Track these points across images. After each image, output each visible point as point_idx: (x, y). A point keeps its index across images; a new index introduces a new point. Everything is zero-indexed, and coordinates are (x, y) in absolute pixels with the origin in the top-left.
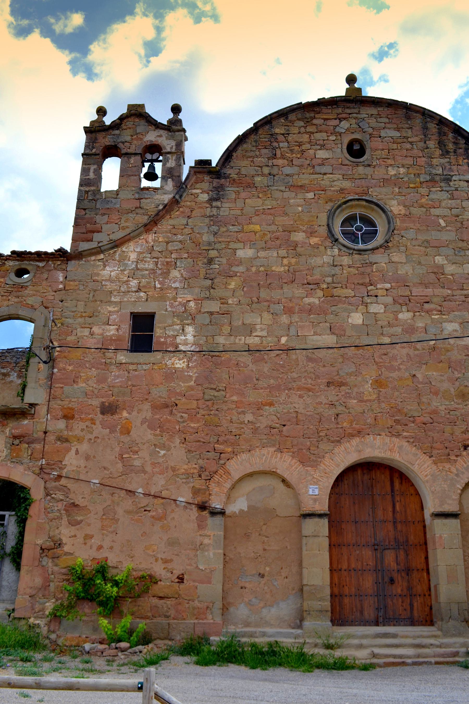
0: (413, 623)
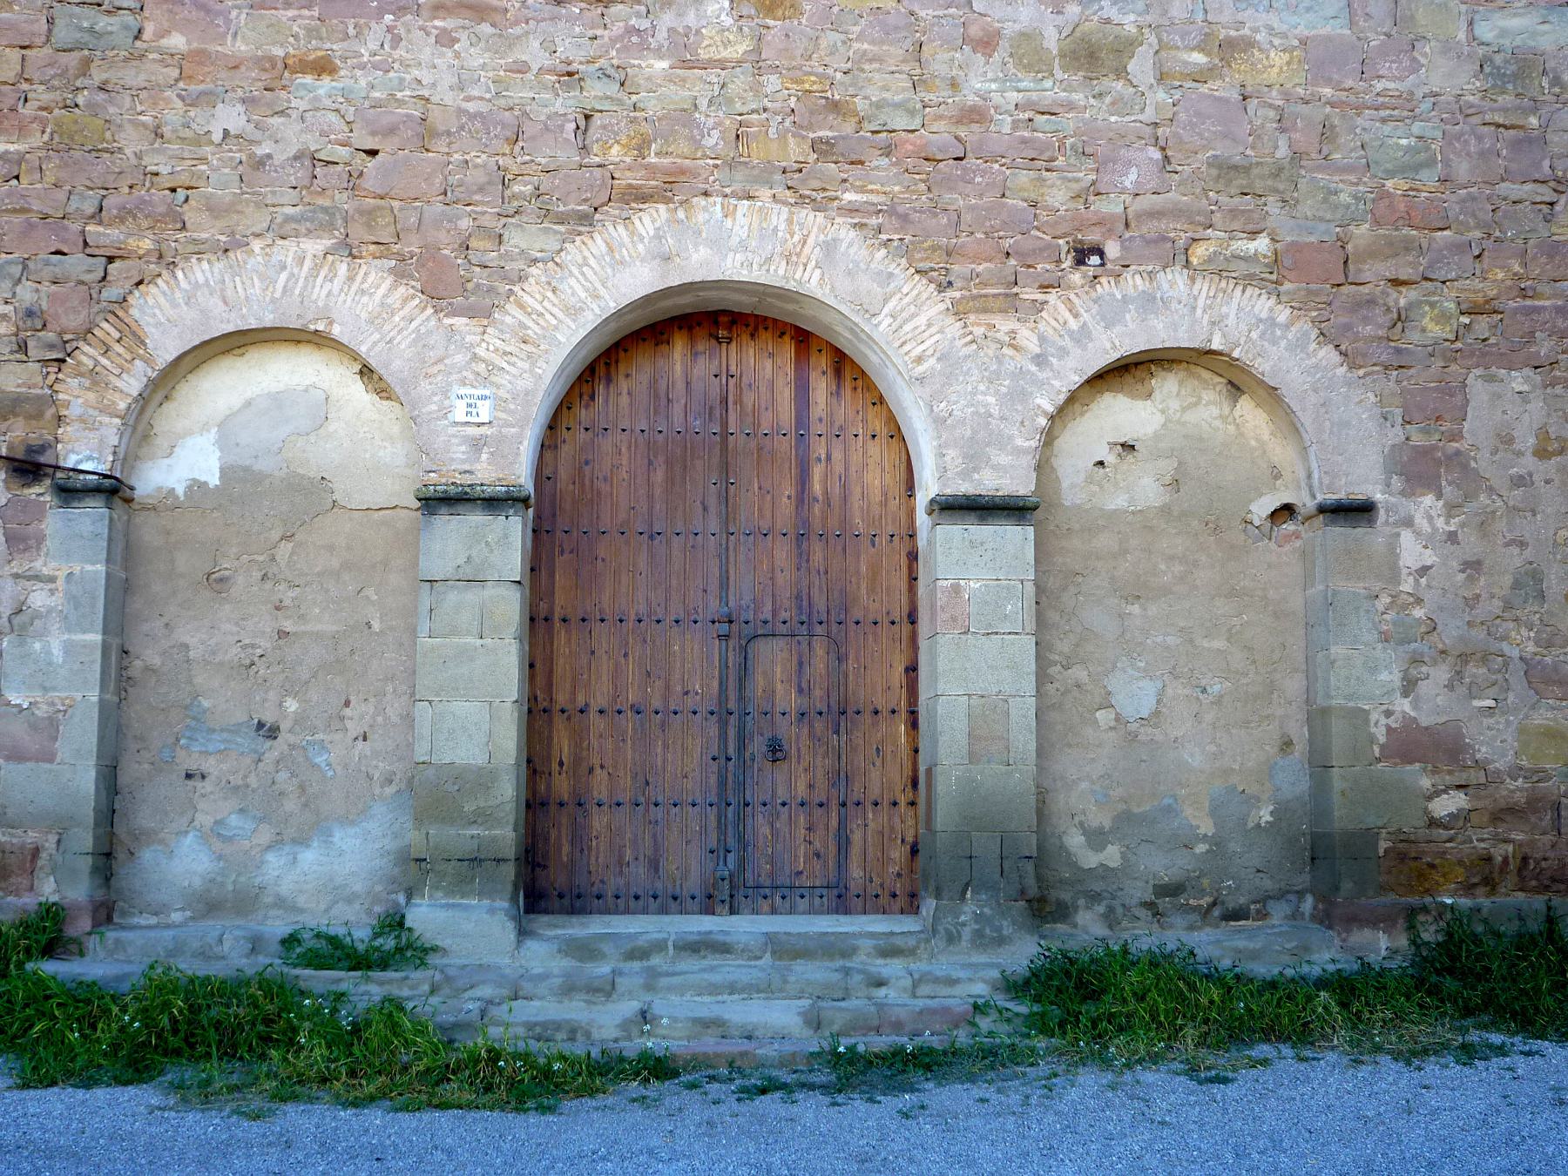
0: (841, 900)
